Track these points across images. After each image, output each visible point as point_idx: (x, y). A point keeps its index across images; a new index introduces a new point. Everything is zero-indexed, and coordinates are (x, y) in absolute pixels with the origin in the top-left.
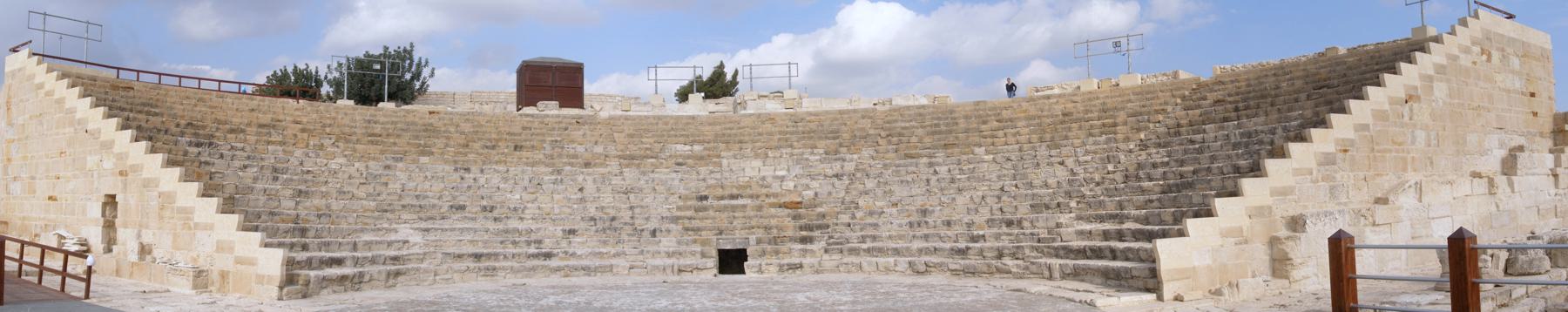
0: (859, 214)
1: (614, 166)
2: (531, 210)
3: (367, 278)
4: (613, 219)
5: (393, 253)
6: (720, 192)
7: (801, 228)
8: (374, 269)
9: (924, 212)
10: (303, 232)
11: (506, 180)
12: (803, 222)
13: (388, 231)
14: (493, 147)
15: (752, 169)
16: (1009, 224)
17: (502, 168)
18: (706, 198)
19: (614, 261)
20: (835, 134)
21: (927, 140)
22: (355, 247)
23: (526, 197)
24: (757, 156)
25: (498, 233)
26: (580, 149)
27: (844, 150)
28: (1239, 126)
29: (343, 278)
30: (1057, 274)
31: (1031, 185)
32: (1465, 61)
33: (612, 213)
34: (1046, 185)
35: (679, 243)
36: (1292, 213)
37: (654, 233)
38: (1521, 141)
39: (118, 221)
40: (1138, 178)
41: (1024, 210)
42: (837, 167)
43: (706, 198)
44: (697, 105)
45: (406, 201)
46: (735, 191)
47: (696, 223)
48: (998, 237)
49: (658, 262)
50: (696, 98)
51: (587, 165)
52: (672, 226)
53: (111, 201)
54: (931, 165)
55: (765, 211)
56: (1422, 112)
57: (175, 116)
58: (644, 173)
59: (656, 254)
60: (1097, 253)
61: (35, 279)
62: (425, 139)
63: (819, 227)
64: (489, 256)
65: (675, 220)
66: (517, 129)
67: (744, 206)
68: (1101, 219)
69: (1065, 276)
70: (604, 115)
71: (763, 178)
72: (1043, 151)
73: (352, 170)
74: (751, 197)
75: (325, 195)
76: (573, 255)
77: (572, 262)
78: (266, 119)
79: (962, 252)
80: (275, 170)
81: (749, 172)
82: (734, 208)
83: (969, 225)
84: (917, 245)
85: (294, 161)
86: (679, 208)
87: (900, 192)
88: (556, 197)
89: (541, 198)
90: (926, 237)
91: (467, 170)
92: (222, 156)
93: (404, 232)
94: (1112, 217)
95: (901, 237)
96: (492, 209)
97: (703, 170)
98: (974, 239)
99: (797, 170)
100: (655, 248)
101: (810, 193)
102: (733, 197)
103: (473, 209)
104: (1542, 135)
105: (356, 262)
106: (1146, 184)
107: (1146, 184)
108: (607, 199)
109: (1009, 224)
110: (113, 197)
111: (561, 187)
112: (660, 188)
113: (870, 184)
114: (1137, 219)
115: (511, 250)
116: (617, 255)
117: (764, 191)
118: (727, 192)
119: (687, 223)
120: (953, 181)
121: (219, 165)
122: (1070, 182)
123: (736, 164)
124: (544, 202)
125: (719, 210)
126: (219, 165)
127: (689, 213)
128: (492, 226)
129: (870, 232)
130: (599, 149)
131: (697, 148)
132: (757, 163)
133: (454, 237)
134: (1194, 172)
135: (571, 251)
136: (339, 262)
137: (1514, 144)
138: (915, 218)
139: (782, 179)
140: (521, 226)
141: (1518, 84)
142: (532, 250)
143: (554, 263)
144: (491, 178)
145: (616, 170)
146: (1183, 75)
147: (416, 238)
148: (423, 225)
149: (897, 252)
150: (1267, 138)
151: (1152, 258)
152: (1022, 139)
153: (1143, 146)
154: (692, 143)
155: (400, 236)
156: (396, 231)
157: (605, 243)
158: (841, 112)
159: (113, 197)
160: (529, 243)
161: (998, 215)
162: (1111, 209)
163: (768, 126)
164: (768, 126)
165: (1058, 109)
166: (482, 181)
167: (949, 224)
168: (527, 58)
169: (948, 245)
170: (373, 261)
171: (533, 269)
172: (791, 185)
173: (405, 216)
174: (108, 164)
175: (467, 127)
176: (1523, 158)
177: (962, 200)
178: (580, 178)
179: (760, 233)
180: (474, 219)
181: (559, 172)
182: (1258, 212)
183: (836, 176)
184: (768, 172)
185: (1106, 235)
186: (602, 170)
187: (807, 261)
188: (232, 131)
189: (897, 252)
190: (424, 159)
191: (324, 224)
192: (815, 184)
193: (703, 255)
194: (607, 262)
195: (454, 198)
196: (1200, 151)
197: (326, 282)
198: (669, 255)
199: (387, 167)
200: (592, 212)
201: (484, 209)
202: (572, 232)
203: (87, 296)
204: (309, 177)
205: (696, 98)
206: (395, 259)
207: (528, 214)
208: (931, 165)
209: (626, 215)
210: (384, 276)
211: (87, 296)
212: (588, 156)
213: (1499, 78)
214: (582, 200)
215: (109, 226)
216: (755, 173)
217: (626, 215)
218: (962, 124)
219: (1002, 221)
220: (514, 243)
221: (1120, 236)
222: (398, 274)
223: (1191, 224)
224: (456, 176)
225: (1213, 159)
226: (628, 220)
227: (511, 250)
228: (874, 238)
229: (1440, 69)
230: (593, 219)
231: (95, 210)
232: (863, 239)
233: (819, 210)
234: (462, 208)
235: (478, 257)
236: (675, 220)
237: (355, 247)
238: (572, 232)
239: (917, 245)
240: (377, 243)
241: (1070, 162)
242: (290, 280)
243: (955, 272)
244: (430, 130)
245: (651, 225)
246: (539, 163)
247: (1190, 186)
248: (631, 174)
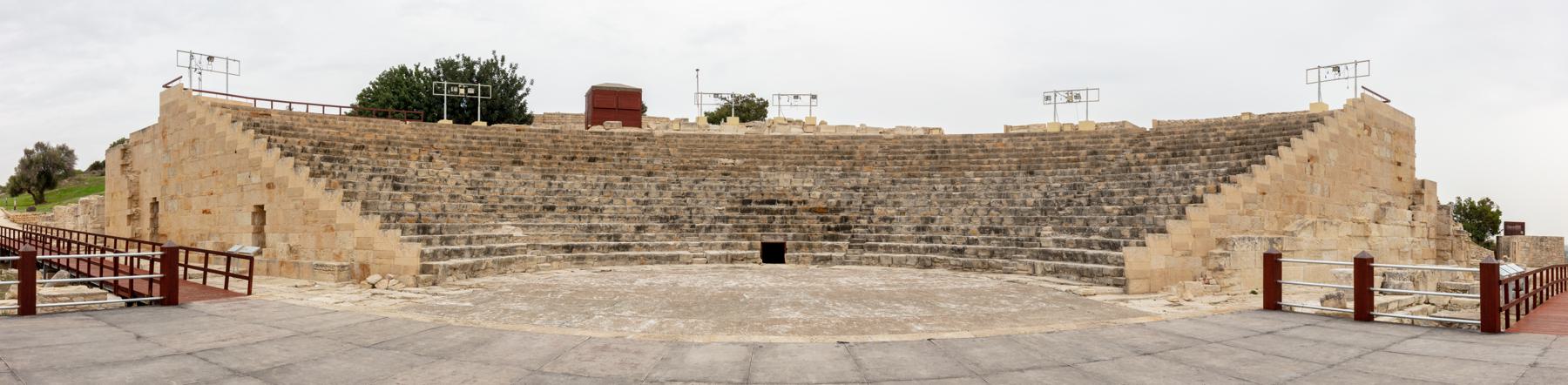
1: (671, 175)
6: (759, 198)
8: (489, 259)
11: (585, 186)
13: (495, 227)
15: (784, 181)
16: (997, 231)
17: (580, 176)
18: (750, 202)
20: (850, 155)
21: (927, 163)
22: (469, 241)
24: (788, 170)
28: (1178, 169)
29: (464, 267)
30: (1039, 271)
31: (1013, 203)
32: (1352, 133)
33: (673, 213)
34: (1025, 203)
36: (1223, 236)
38: (1390, 199)
39: (266, 228)
40: (1099, 203)
41: (1008, 221)
42: (853, 181)
43: (750, 202)
44: (732, 126)
45: (505, 204)
47: (743, 222)
48: (988, 241)
50: (733, 120)
51: (650, 174)
53: (260, 211)
54: (930, 183)
55: (798, 215)
57: (308, 137)
59: (711, 247)
60: (1072, 257)
61: (200, 281)
62: (517, 154)
64: (578, 247)
65: (726, 219)
66: (589, 144)
68: (1072, 231)
69: (1045, 273)
70: (658, 133)
72: (1020, 178)
75: (439, 198)
78: (382, 138)
79: (961, 252)
80: (395, 179)
83: (965, 231)
85: (411, 173)
87: (906, 204)
90: (930, 240)
91: (553, 178)
92: (351, 169)
94: (1080, 230)
95: (910, 239)
97: (744, 179)
98: (969, 242)
99: (821, 183)
101: (833, 201)
104: (1404, 195)
105: (472, 253)
106: (1107, 208)
107: (1107, 208)
109: (997, 231)
110: (262, 207)
113: (881, 196)
114: (1101, 234)
115: (596, 243)
120: (949, 196)
121: (352, 177)
122: (1046, 203)
123: (772, 176)
125: (759, 212)
126: (352, 177)
128: (576, 222)
129: (884, 233)
130: (658, 162)
131: (738, 161)
132: (788, 176)
137: (1384, 201)
138: (920, 224)
139: (810, 189)
141: (1386, 153)
144: (573, 183)
147: (519, 233)
148: (523, 222)
149: (908, 250)
150: (1201, 179)
151: (1120, 262)
159: (262, 207)
161: (987, 224)
162: (1080, 224)
163: (794, 147)
166: (566, 187)
167: (948, 229)
168: (598, 82)
169: (949, 246)
170: (488, 252)
171: (616, 258)
172: (818, 194)
173: (508, 215)
174: (256, 179)
175: (548, 142)
176: (1391, 211)
177: (956, 212)
181: (628, 179)
184: (798, 183)
185: (1078, 244)
186: (662, 179)
187: (836, 254)
188: (355, 148)
189: (908, 250)
190: (517, 169)
191: (442, 222)
192: (836, 194)
193: (751, 247)
195: (545, 200)
196: (1149, 184)
198: (724, 246)
199: (487, 175)
201: (570, 209)
203: (249, 293)
204: (424, 184)
205: (733, 120)
207: (606, 213)
208: (930, 183)
209: (685, 215)
211: (249, 293)
212: (650, 167)
213: (1376, 149)
215: (259, 232)
216: (787, 184)
217: (685, 215)
218: (953, 152)
221: (1089, 245)
223: (1150, 238)
224: (544, 183)
225: (1159, 191)
227: (596, 243)
228: (887, 239)
229: (1334, 138)
231: (246, 219)
232: (879, 239)
234: (552, 208)
235: (569, 249)
236: (726, 219)
237: (469, 241)
239: (922, 245)
241: (1043, 187)
243: (955, 268)
245: (706, 223)
247: (1139, 210)
248: (687, 181)
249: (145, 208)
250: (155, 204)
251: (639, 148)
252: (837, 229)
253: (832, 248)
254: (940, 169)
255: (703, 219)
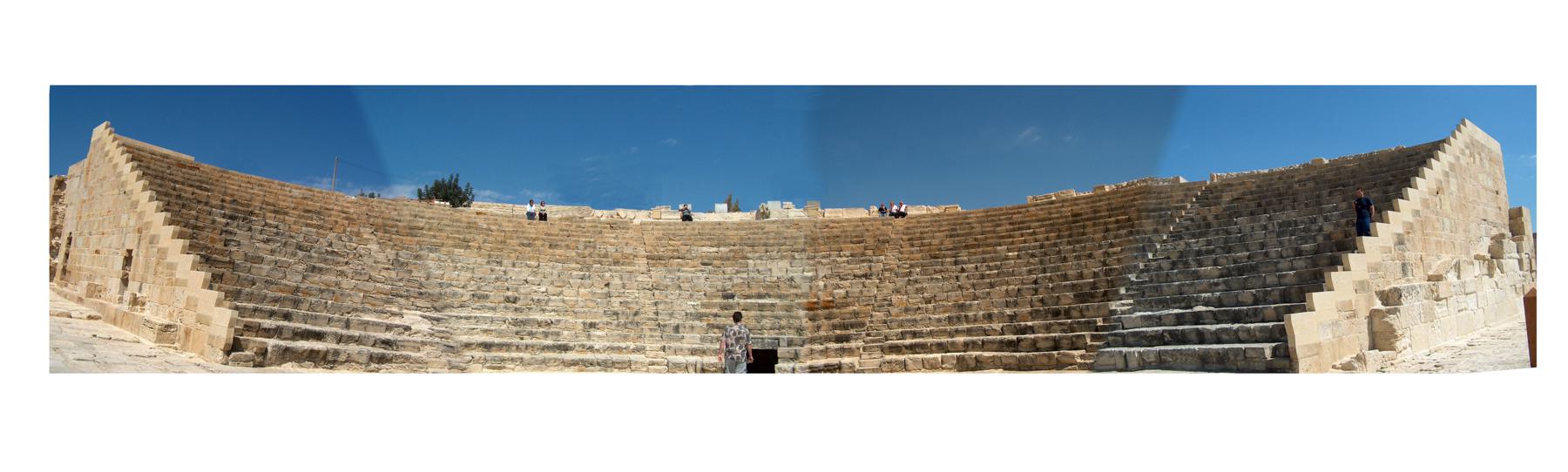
0: (894, 311)
1: (642, 264)
2: (555, 302)
3: (342, 358)
4: (636, 314)
5: (388, 336)
7: (835, 327)
9: (962, 307)
10: (296, 303)
11: (535, 274)
12: (836, 321)
13: (393, 314)
14: (529, 245)
16: (1056, 314)
17: (534, 263)
18: (732, 296)
19: (633, 357)
22: (347, 325)
23: (551, 289)
25: (516, 323)
26: (611, 249)
27: (870, 252)
31: (1065, 277)
35: (703, 340)
37: (677, 329)
46: (762, 291)
49: (680, 359)
51: (616, 263)
52: (697, 323)
56: (1447, 202)
58: (670, 272)
63: (852, 326)
64: (501, 346)
67: (773, 305)
71: (792, 279)
73: (381, 257)
74: (780, 297)
76: (591, 348)
77: (589, 356)
81: (776, 273)
82: (761, 307)
84: (961, 339)
86: (703, 305)
87: (931, 288)
88: (582, 290)
89: (566, 291)
93: (412, 318)
96: (515, 300)
100: (678, 344)
101: (842, 292)
102: (760, 296)
103: (496, 296)
108: (633, 294)
111: (587, 282)
112: (686, 286)
116: (637, 350)
117: (793, 291)
118: (754, 291)
119: (712, 320)
120: (983, 277)
124: (569, 294)
127: (715, 311)
128: (510, 316)
132: (784, 264)
133: (464, 325)
134: (1249, 257)
135: (589, 343)
136: (319, 336)
140: (539, 317)
142: (549, 342)
143: (569, 356)
144: (519, 273)
145: (643, 269)
146: (1182, 180)
147: (425, 326)
152: (1040, 237)
153: (1176, 236)
154: (718, 246)
155: (406, 321)
156: (401, 315)
157: (625, 338)
158: (862, 220)
160: (546, 335)
163: (793, 231)
164: (793, 231)
165: (1067, 211)
171: (544, 362)
172: (821, 284)
178: (608, 275)
179: (792, 335)
180: (494, 309)
182: (1361, 287)
183: (865, 276)
185: (1180, 319)
194: (625, 357)
197: (286, 355)
198: (693, 352)
200: (616, 306)
201: (508, 300)
202: (592, 325)
206: (387, 343)
210: (364, 359)
214: (609, 295)
218: (978, 229)
219: (1047, 312)
220: (531, 334)
222: (382, 359)
226: (652, 316)
228: (914, 335)
230: (616, 314)
232: (903, 336)
233: (851, 308)
235: (487, 346)
236: (700, 317)
238: (592, 325)
239: (961, 339)
240: (378, 324)
242: (234, 346)
243: (1008, 368)
244: (471, 226)
245: (674, 322)
246: (566, 260)
248: (658, 273)
249: (63, 241)
250: (70, 239)
251: (609, 236)
252: (845, 327)
253: (842, 352)
254: (967, 247)
255: (671, 315)
